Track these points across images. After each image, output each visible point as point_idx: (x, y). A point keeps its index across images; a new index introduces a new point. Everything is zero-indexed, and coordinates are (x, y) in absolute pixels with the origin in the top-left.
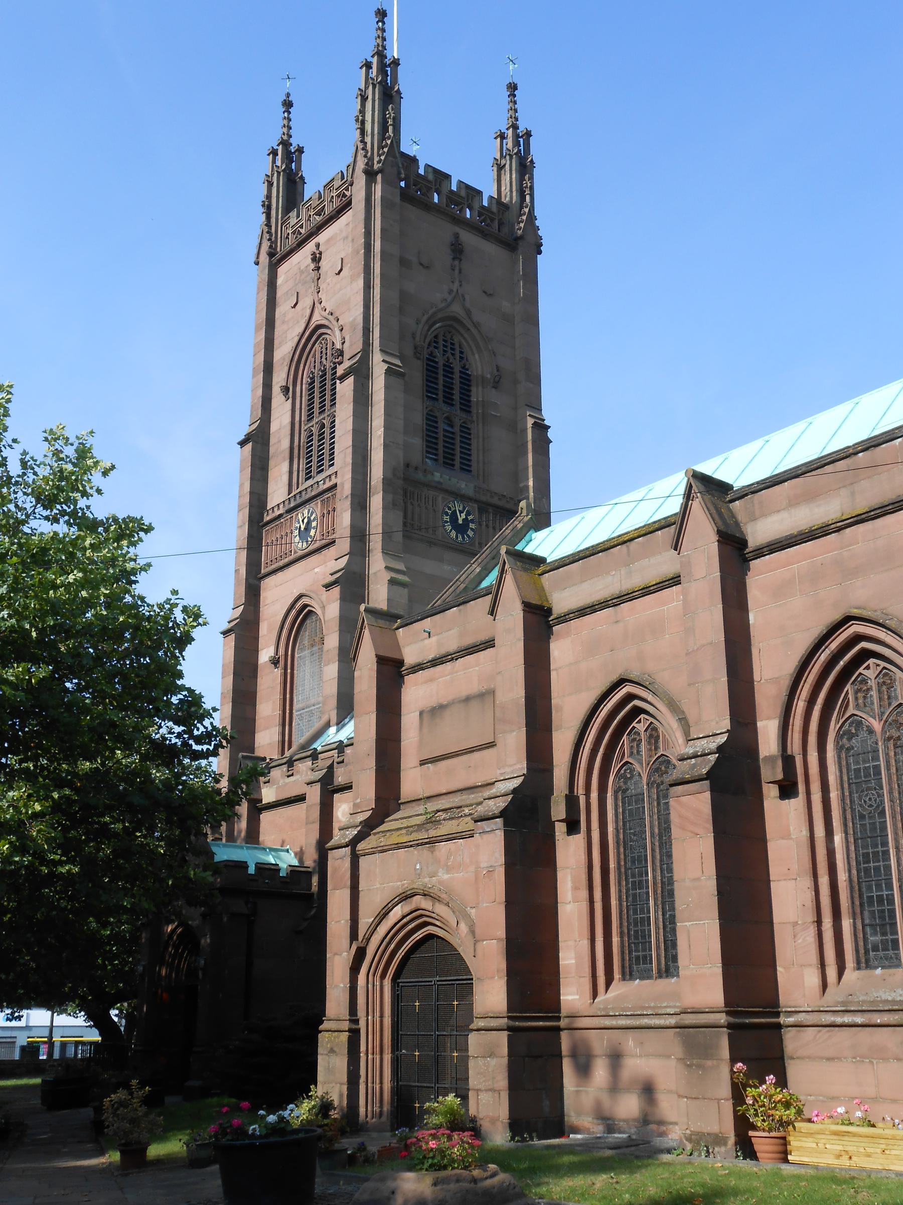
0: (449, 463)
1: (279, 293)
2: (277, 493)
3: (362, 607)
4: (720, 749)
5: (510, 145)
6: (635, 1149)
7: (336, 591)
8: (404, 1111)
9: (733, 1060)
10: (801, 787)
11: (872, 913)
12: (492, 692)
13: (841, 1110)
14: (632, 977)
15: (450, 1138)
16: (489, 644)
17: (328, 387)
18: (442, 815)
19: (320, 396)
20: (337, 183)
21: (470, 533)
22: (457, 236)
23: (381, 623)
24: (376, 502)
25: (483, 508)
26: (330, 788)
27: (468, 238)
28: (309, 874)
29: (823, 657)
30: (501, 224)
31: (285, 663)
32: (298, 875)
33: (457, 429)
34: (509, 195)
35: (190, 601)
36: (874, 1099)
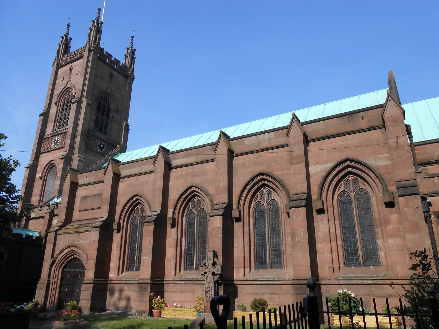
0: (100, 131)
1: (58, 76)
2: (49, 131)
3: (69, 167)
4: (158, 215)
5: (130, 52)
6: (124, 314)
7: (63, 161)
8: (60, 305)
9: (151, 292)
10: (176, 226)
11: (189, 257)
12: (102, 194)
13: (175, 304)
14: (129, 271)
15: (71, 312)
16: (103, 182)
17: (69, 104)
18: (83, 225)
19: (66, 106)
20: (80, 50)
21: (104, 150)
22: (112, 72)
23: (73, 172)
24: (78, 138)
25: (109, 144)
26: (52, 215)
27: (114, 73)
28: (42, 239)
29: (185, 195)
30: (124, 71)
31: (44, 179)
32: (39, 239)
33: (104, 122)
34: (128, 64)
35: (16, 159)
36: (184, 302)
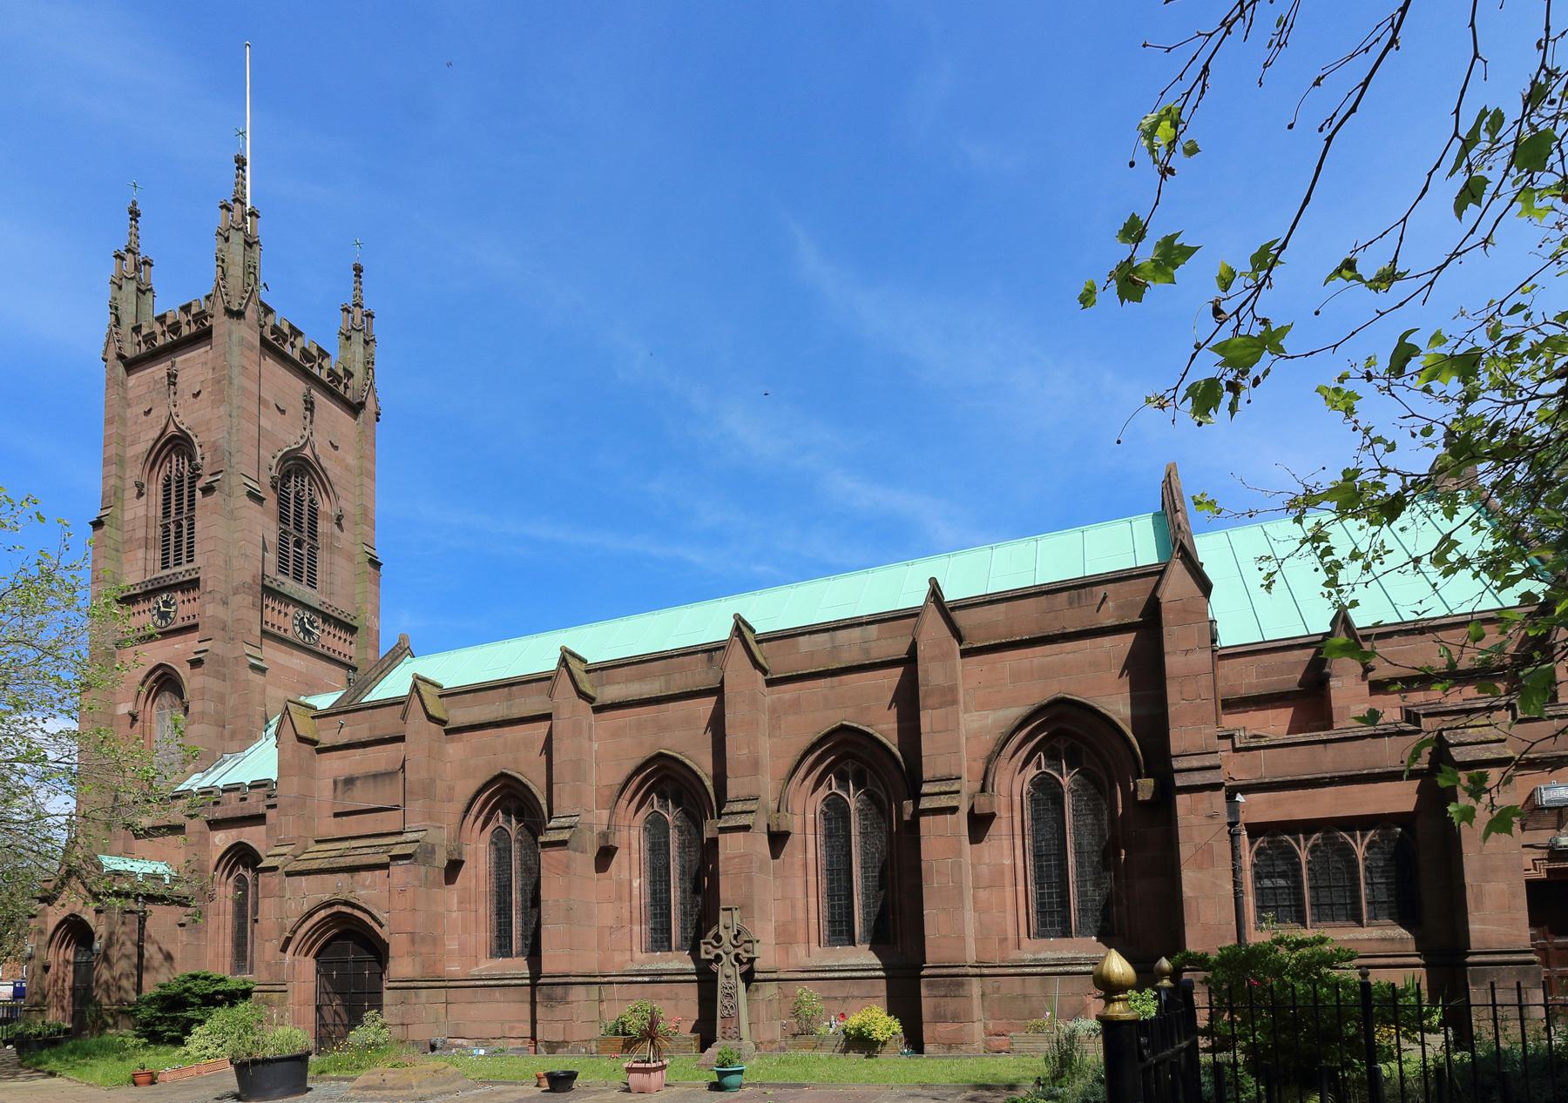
0: (298, 577)
27: (319, 397)
